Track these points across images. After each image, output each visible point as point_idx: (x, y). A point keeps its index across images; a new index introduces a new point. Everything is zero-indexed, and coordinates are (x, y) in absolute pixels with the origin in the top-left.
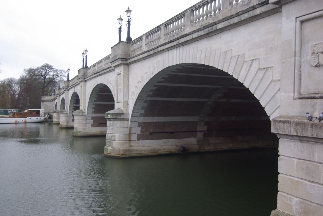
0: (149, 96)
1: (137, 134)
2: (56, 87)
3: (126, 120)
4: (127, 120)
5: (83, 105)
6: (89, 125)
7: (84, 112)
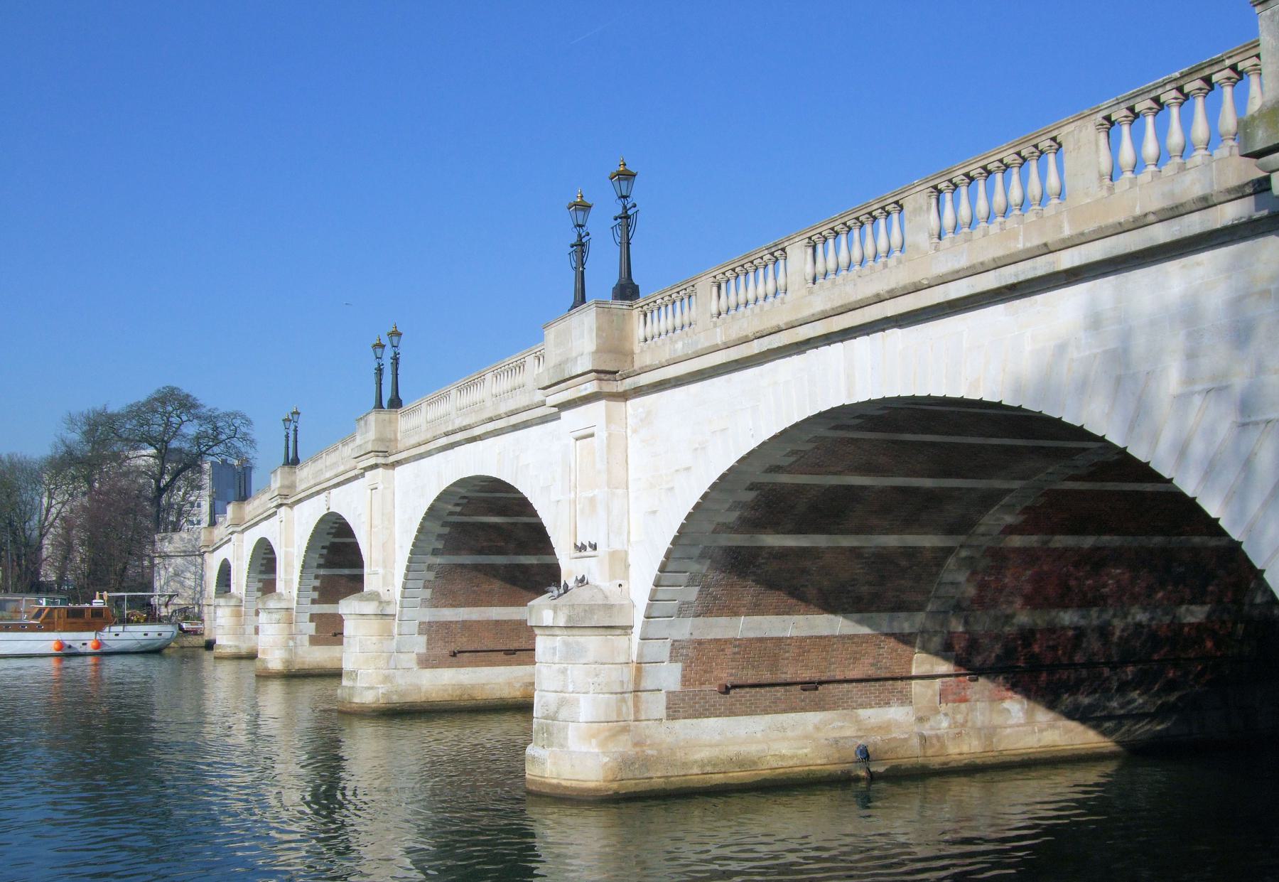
2: (200, 488)
3: (619, 632)
4: (627, 629)
5: (381, 571)
6: (409, 660)
7: (388, 603)
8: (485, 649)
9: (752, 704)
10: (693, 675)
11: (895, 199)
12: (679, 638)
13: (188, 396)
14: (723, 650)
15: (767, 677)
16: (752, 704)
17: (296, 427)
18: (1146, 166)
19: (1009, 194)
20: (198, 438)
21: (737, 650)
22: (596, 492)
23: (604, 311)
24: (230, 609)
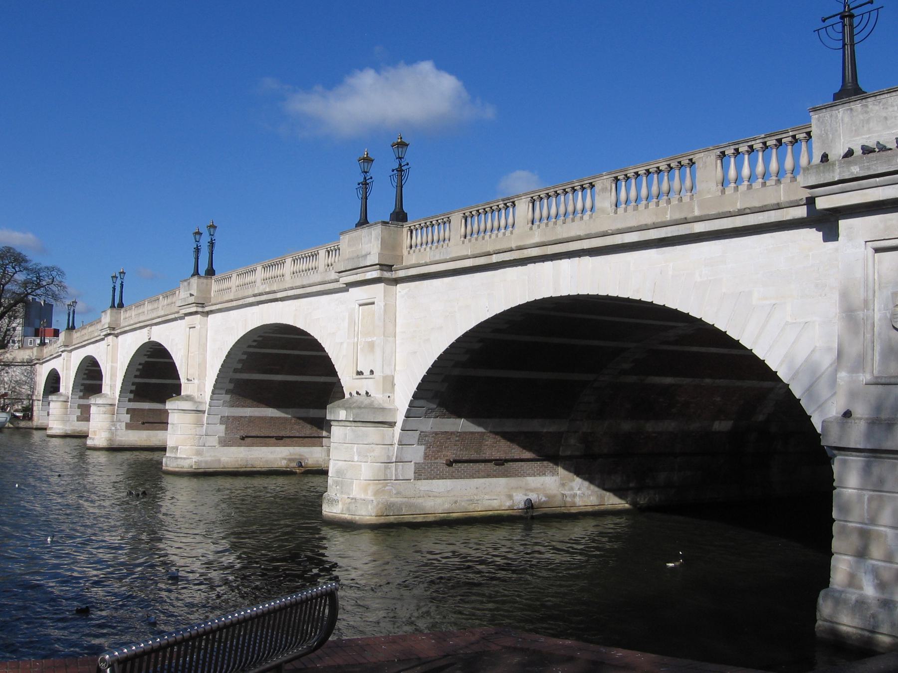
0: (236, 371)
1: (415, 463)
4: (392, 424)
6: (213, 441)
8: (263, 435)
9: (465, 472)
10: (431, 453)
11: (590, 181)
12: (424, 431)
13: (20, 254)
14: (449, 439)
15: (474, 456)
16: (465, 472)
17: (122, 282)
18: (758, 178)
19: (629, 193)
20: (25, 284)
21: (457, 438)
22: (375, 339)
23: (386, 228)
24: (59, 404)
